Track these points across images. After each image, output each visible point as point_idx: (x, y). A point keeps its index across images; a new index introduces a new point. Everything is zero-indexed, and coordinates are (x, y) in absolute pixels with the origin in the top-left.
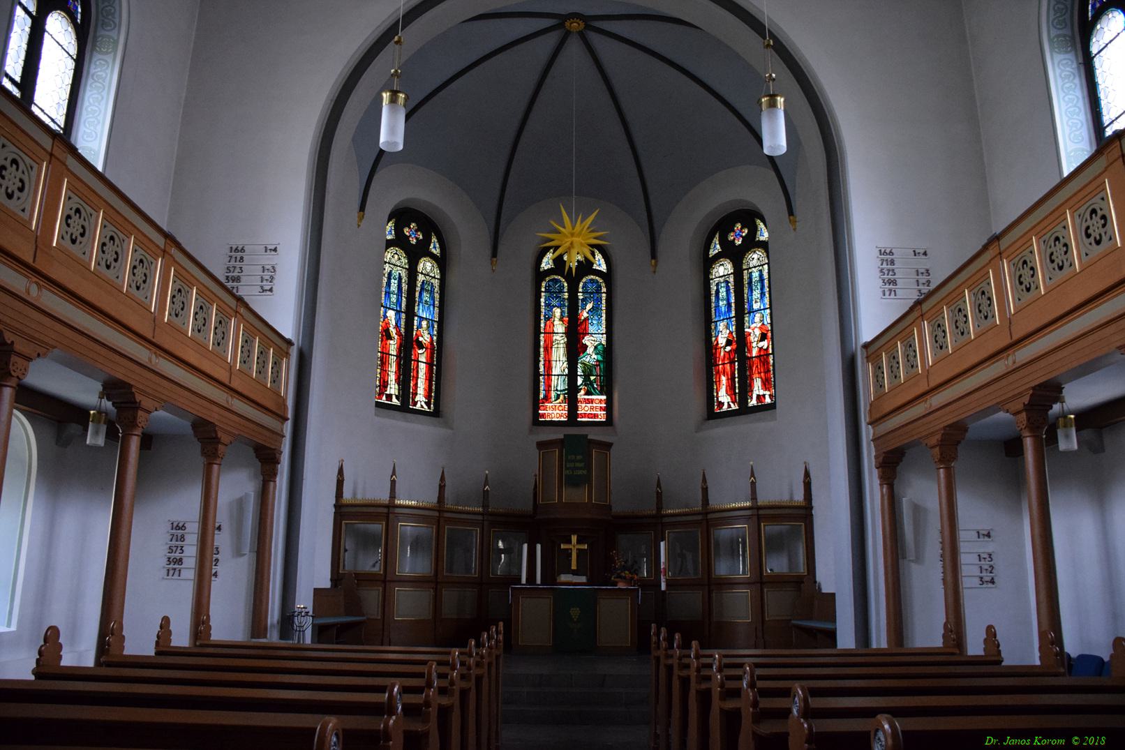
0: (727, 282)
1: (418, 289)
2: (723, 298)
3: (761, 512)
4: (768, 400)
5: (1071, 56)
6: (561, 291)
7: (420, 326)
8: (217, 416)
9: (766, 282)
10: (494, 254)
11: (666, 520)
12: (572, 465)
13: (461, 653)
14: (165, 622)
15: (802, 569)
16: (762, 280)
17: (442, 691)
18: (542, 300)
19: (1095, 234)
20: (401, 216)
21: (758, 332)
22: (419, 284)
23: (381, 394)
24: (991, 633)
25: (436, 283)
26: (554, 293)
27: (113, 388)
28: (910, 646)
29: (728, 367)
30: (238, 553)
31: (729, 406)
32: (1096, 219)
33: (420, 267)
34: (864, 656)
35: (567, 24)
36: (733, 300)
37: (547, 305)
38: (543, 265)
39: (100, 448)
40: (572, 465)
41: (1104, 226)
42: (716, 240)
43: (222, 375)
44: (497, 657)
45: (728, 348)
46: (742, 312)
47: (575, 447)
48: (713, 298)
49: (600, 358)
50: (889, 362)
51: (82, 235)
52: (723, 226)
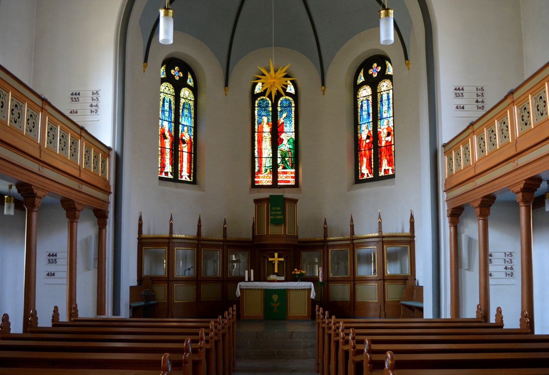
0: (368, 100)
1: (181, 108)
2: (366, 109)
4: (391, 173)
6: (267, 106)
7: (183, 130)
12: (274, 213)
14: (56, 309)
15: (408, 272)
16: (388, 99)
18: (256, 112)
21: (386, 131)
22: (181, 104)
23: (161, 172)
24: (499, 311)
25: (192, 103)
27: (21, 186)
28: (464, 317)
29: (367, 152)
30: (88, 269)
31: (368, 176)
33: (182, 95)
34: (438, 323)
36: (371, 111)
37: (259, 115)
38: (255, 91)
40: (274, 213)
42: (362, 74)
43: (76, 173)
44: (233, 323)
45: (368, 141)
46: (376, 118)
47: (276, 204)
48: (359, 110)
49: (291, 147)
50: (456, 157)
52: (366, 65)
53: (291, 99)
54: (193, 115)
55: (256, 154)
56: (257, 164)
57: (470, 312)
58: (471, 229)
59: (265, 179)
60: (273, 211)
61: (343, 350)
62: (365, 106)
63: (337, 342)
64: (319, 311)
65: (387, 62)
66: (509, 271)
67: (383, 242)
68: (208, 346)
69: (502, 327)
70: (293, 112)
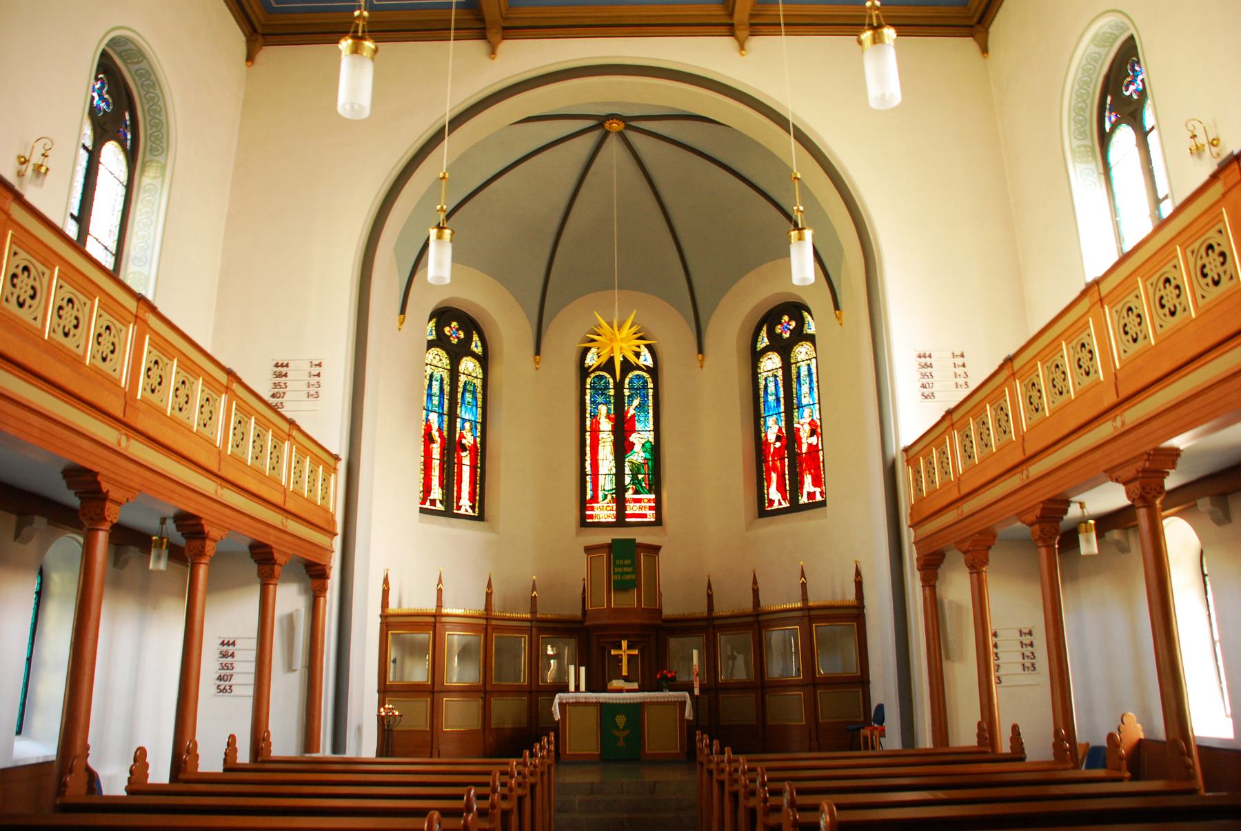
0: (776, 376)
1: (460, 390)
2: (772, 390)
3: (812, 613)
4: (819, 498)
5: (1092, 166)
6: (607, 388)
7: (463, 428)
8: (272, 538)
9: (814, 376)
10: (538, 352)
11: (717, 622)
12: (620, 570)
13: (518, 764)
14: (232, 737)
16: (810, 374)
17: (504, 797)
18: (588, 397)
19: (1169, 305)
20: (442, 315)
21: (807, 428)
22: (461, 385)
23: (423, 502)
24: (1015, 729)
25: (479, 383)
26: (600, 390)
32: (1170, 288)
33: (462, 368)
34: (909, 754)
35: (607, 125)
36: (781, 395)
37: (593, 402)
39: (161, 571)
40: (620, 570)
41: (1178, 296)
42: (764, 333)
43: (277, 498)
44: (549, 766)
45: (778, 445)
48: (762, 393)
49: (648, 456)
50: (926, 468)
51: (33, 297)
52: (771, 318)
53: (646, 375)
54: (480, 403)
55: (588, 469)
56: (589, 486)
57: (965, 734)
58: (956, 587)
59: (603, 512)
60: (619, 566)
61: (745, 807)
62: (771, 388)
63: (735, 795)
64: (703, 740)
65: (805, 314)
66: (1028, 662)
67: (810, 617)
68: (505, 805)
69: (1022, 759)
70: (650, 398)
